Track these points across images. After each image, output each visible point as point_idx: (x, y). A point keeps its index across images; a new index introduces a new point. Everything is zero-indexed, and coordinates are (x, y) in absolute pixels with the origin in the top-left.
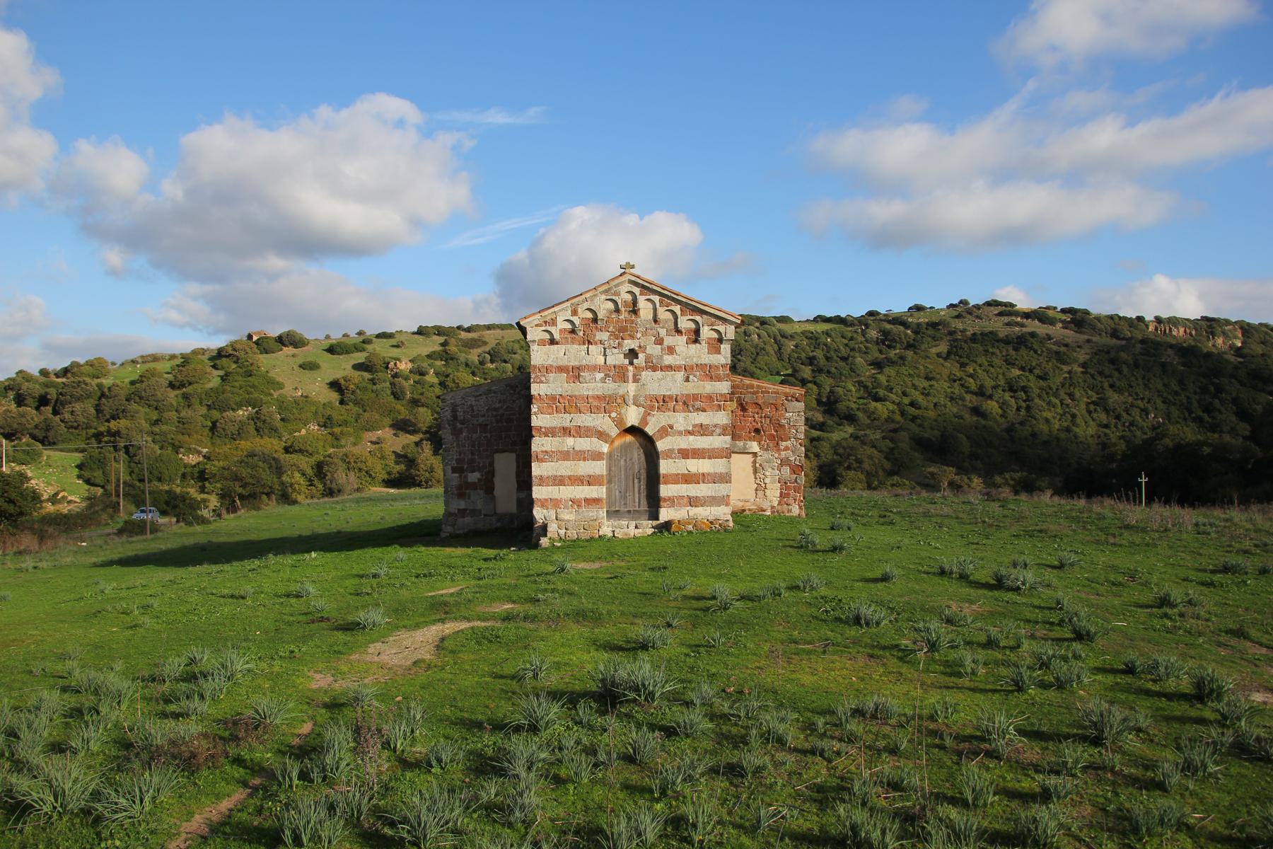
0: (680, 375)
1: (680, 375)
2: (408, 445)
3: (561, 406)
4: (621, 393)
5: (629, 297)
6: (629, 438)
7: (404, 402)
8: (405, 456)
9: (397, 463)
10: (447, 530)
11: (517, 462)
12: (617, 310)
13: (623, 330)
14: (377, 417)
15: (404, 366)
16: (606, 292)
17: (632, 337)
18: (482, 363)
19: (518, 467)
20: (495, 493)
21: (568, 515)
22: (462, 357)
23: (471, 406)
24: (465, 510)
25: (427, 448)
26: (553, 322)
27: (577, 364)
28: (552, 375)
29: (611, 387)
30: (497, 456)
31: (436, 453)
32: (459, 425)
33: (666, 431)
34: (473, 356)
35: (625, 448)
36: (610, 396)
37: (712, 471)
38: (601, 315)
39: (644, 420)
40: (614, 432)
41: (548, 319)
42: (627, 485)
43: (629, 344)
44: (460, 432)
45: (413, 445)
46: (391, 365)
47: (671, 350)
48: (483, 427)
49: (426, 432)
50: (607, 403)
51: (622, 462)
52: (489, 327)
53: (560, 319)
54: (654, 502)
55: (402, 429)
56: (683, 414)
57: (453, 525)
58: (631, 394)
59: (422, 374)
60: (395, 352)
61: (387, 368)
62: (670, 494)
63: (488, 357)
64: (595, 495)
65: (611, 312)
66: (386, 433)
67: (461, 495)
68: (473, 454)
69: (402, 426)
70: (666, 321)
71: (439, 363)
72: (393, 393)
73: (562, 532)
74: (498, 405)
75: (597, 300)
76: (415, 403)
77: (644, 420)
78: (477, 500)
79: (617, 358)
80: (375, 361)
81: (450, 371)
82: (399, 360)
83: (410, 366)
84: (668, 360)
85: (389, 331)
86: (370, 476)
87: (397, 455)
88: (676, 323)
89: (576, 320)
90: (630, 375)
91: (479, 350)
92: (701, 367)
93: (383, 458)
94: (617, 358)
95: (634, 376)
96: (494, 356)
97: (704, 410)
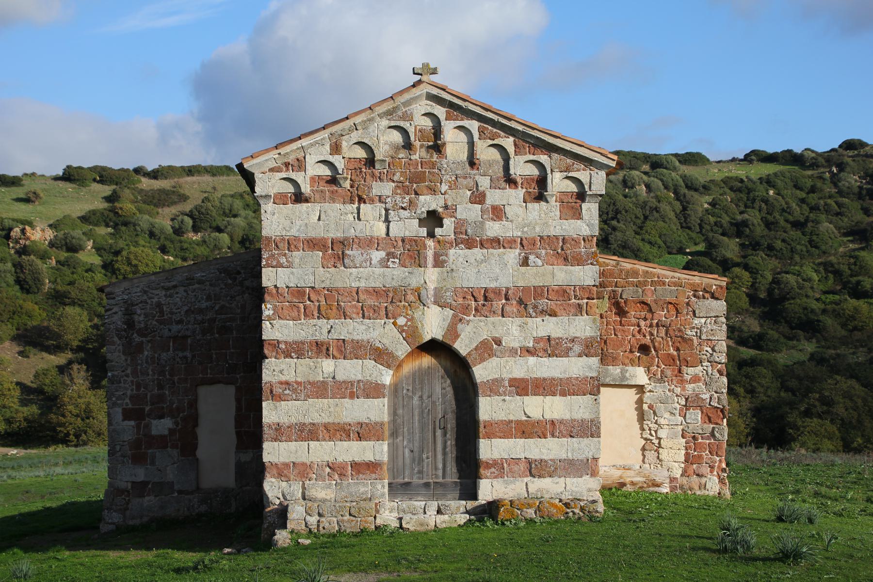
0: (513, 255)
1: (513, 255)
2: (45, 372)
3: (313, 307)
5: (428, 123)
6: (427, 361)
7: (39, 297)
8: (39, 391)
9: (24, 403)
11: (238, 401)
12: (408, 145)
13: (418, 178)
16: (389, 113)
17: (433, 191)
18: (178, 231)
19: (239, 409)
20: (201, 453)
22: (144, 221)
23: (159, 305)
24: (144, 484)
25: (80, 377)
26: (300, 165)
27: (339, 235)
29: (396, 275)
32: (137, 338)
36: (395, 290)
37: (567, 417)
39: (453, 331)
40: (402, 349)
41: (291, 159)
42: (423, 439)
43: (428, 202)
44: (140, 348)
45: (54, 372)
46: (16, 232)
47: (498, 213)
49: (79, 349)
51: (416, 401)
53: (311, 160)
54: (469, 469)
56: (518, 321)
58: (431, 286)
59: (73, 248)
60: (23, 211)
61: (8, 237)
64: (369, 457)
65: (397, 148)
67: (138, 459)
68: (161, 387)
70: (490, 164)
71: (103, 231)
72: (18, 281)
73: (313, 520)
74: (204, 304)
75: (373, 128)
76: (59, 298)
77: (453, 331)
78: (167, 466)
79: (407, 226)
81: (121, 244)
82: (30, 224)
83: (50, 234)
84: (494, 229)
88: (506, 168)
90: (430, 254)
92: (547, 240)
94: (407, 226)
95: (436, 256)
97: (553, 314)
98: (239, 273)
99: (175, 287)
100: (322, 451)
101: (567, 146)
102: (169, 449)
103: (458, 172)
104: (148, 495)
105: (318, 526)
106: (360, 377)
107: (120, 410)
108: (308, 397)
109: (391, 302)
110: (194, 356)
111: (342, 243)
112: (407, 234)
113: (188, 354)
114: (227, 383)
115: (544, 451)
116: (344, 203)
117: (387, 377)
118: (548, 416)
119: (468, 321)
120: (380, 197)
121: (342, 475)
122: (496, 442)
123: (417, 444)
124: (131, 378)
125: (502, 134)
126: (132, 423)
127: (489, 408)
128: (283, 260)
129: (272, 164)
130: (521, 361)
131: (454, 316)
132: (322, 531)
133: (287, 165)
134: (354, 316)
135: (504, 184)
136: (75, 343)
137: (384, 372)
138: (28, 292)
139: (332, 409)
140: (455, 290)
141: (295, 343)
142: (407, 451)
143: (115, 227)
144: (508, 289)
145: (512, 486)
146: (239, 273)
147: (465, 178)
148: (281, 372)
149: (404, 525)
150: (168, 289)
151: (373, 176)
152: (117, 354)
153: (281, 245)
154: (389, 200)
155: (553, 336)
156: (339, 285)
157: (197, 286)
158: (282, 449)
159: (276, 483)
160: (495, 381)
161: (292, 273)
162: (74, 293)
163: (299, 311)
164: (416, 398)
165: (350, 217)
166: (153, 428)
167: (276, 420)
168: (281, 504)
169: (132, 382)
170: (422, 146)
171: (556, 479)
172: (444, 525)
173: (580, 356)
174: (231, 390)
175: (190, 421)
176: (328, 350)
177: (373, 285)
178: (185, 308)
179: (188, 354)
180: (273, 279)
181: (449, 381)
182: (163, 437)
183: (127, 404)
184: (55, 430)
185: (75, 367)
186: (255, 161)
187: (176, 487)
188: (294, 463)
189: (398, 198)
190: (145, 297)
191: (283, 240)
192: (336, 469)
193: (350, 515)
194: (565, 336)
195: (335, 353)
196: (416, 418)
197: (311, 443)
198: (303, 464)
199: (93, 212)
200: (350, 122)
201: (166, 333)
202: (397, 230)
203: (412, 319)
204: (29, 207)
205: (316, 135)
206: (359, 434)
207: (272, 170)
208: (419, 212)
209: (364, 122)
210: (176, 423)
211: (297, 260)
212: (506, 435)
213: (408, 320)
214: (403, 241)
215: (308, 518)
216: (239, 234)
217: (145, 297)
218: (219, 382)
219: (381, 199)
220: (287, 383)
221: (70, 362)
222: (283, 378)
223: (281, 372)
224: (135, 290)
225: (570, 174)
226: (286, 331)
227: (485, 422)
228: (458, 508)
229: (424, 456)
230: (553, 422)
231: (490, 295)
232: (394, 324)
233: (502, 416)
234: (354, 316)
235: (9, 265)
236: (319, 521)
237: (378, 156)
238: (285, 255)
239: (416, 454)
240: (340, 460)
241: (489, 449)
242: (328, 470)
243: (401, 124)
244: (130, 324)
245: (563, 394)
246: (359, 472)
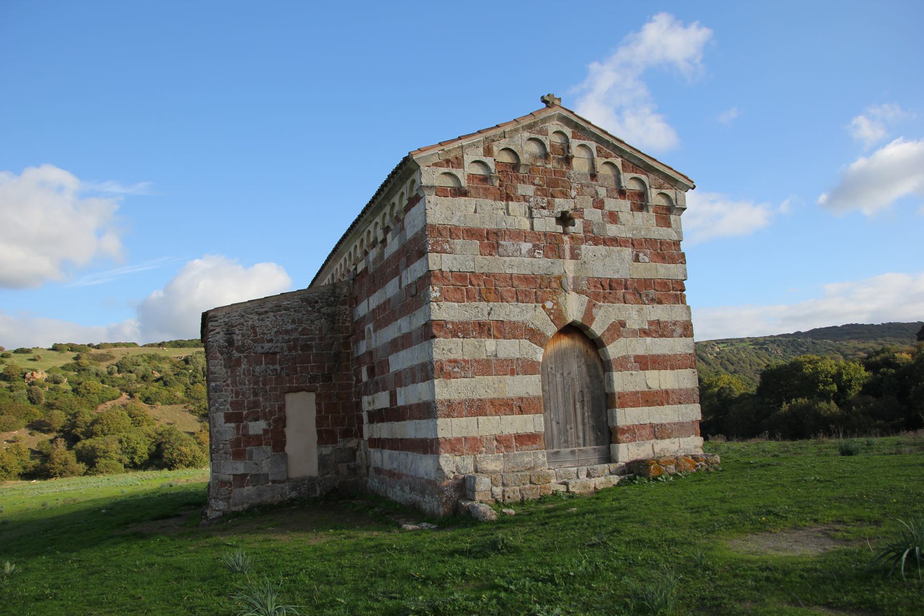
0: (628, 252)
1: (628, 252)
2: (43, 443)
3: (474, 290)
4: (557, 273)
5: (557, 140)
6: (565, 342)
7: (40, 406)
8: (40, 452)
9: (32, 458)
10: (218, 507)
11: (318, 404)
12: (546, 156)
13: (553, 184)
14: (14, 419)
15: (41, 376)
16: (530, 127)
17: (565, 195)
18: (110, 373)
19: (319, 411)
20: (288, 449)
21: (493, 463)
22: (93, 368)
23: (253, 327)
24: (244, 476)
25: (62, 444)
26: (458, 162)
27: (493, 227)
28: (458, 243)
29: (541, 264)
30: (289, 398)
31: (69, 448)
32: (236, 354)
33: (618, 329)
34: (103, 367)
35: (561, 356)
36: (542, 278)
37: (676, 387)
38: (524, 159)
39: (589, 315)
40: (551, 330)
41: (451, 156)
42: (566, 412)
43: (562, 205)
44: (238, 362)
45: (48, 443)
46: (29, 375)
47: (613, 217)
48: (270, 356)
49: (60, 431)
50: (540, 288)
51: (559, 378)
52: (116, 345)
53: (468, 159)
54: (607, 436)
55: (37, 429)
56: (636, 307)
57: (227, 499)
58: (571, 275)
59: (57, 382)
60: (32, 365)
61: (24, 377)
62: (629, 423)
63: (116, 368)
64: (530, 429)
65: (536, 158)
66: (22, 433)
67: (238, 455)
68: (256, 394)
69: (37, 427)
70: (605, 178)
71: (72, 373)
72: (29, 399)
73: (498, 490)
74: (290, 327)
75: (517, 137)
76: (50, 406)
77: (589, 315)
78: (262, 460)
79: (547, 224)
80: (13, 371)
81: (82, 379)
82: (36, 371)
83: (46, 375)
84: (612, 230)
85: (26, 347)
86: (6, 470)
87: (33, 452)
88: (618, 181)
89: (489, 161)
90: (567, 247)
91: (108, 363)
92: (650, 242)
93: (19, 454)
94: (547, 224)
95: (572, 249)
96: (120, 367)
97: (660, 302)
98: (317, 302)
99: (266, 312)
100: (490, 426)
101: (661, 168)
102: (263, 446)
103: (583, 182)
104: (247, 485)
105: (504, 496)
106: (518, 356)
107: (222, 414)
108: (475, 374)
109: (540, 288)
110: (282, 369)
111: (496, 234)
112: (548, 229)
113: (278, 367)
114: (309, 391)
115: (663, 416)
116: (495, 200)
117: (539, 355)
118: (663, 387)
119: (601, 306)
120: (524, 196)
121: (508, 447)
122: (628, 410)
123: (561, 416)
124: (231, 388)
125: (613, 154)
126: (233, 425)
127: (621, 381)
128: (446, 246)
129: (436, 159)
130: (641, 340)
131: (589, 302)
132: (508, 501)
133: (448, 161)
134: (509, 299)
135: (616, 195)
136: (58, 428)
137: (538, 351)
138: (34, 403)
139: (496, 386)
140: (588, 279)
141: (461, 323)
142: (554, 423)
143: (79, 371)
144: (626, 280)
145: (642, 448)
146: (317, 302)
147: (588, 187)
148: (450, 350)
149: (571, 489)
150: (259, 314)
151: (517, 178)
152: (219, 367)
153: (444, 233)
154: (531, 199)
155: (662, 320)
156: (495, 271)
157: (283, 312)
158: (454, 425)
159: (451, 458)
160: (624, 357)
161: (455, 259)
162: (58, 403)
163: (462, 294)
164: (558, 375)
165: (501, 212)
166: (250, 429)
167: (447, 397)
168: (455, 478)
169: (232, 390)
170: (554, 158)
171: (673, 440)
172: (602, 487)
173: (681, 336)
174: (312, 396)
175: (280, 422)
176: (489, 330)
177: (524, 272)
178: (275, 330)
179: (278, 367)
180: (438, 263)
181: (583, 360)
182: (258, 436)
183: (228, 409)
184: (48, 471)
185: (59, 439)
186: (423, 154)
187: (270, 478)
188: (465, 438)
189: (539, 199)
190: (242, 320)
191: (446, 228)
192: (503, 442)
193: (531, 482)
194: (669, 320)
195: (496, 333)
196: (560, 393)
197: (480, 418)
198: (474, 438)
199: (68, 365)
200: (500, 130)
201: (259, 350)
202: (539, 225)
203: (557, 304)
204: (36, 363)
205: (473, 137)
206: (520, 407)
207: (436, 165)
208: (556, 211)
209: (511, 131)
210: (269, 425)
211: (458, 247)
212: (636, 405)
213: (555, 304)
214: (545, 235)
215: (494, 489)
216: (141, 374)
217: (242, 320)
218: (303, 390)
219: (525, 198)
220: (455, 361)
221: (56, 438)
222: (452, 357)
223: (450, 350)
224: (234, 314)
225: (663, 191)
226: (452, 313)
227: (619, 393)
228: (604, 470)
229: (568, 427)
230: (667, 392)
231: (614, 285)
232: (544, 307)
233: (631, 388)
234: (509, 299)
235: (25, 391)
236: (504, 491)
237: (523, 161)
238: (448, 242)
239: (561, 426)
240: (506, 433)
241: (624, 417)
242: (495, 443)
243: (540, 137)
244: (230, 342)
245: (672, 368)
246: (522, 444)
